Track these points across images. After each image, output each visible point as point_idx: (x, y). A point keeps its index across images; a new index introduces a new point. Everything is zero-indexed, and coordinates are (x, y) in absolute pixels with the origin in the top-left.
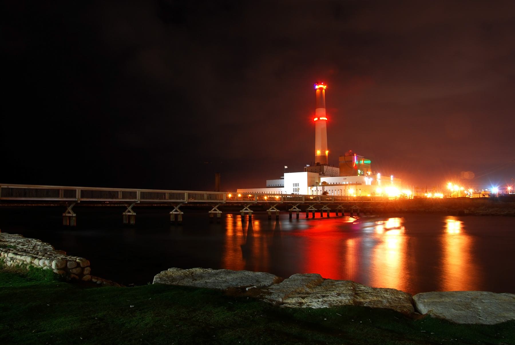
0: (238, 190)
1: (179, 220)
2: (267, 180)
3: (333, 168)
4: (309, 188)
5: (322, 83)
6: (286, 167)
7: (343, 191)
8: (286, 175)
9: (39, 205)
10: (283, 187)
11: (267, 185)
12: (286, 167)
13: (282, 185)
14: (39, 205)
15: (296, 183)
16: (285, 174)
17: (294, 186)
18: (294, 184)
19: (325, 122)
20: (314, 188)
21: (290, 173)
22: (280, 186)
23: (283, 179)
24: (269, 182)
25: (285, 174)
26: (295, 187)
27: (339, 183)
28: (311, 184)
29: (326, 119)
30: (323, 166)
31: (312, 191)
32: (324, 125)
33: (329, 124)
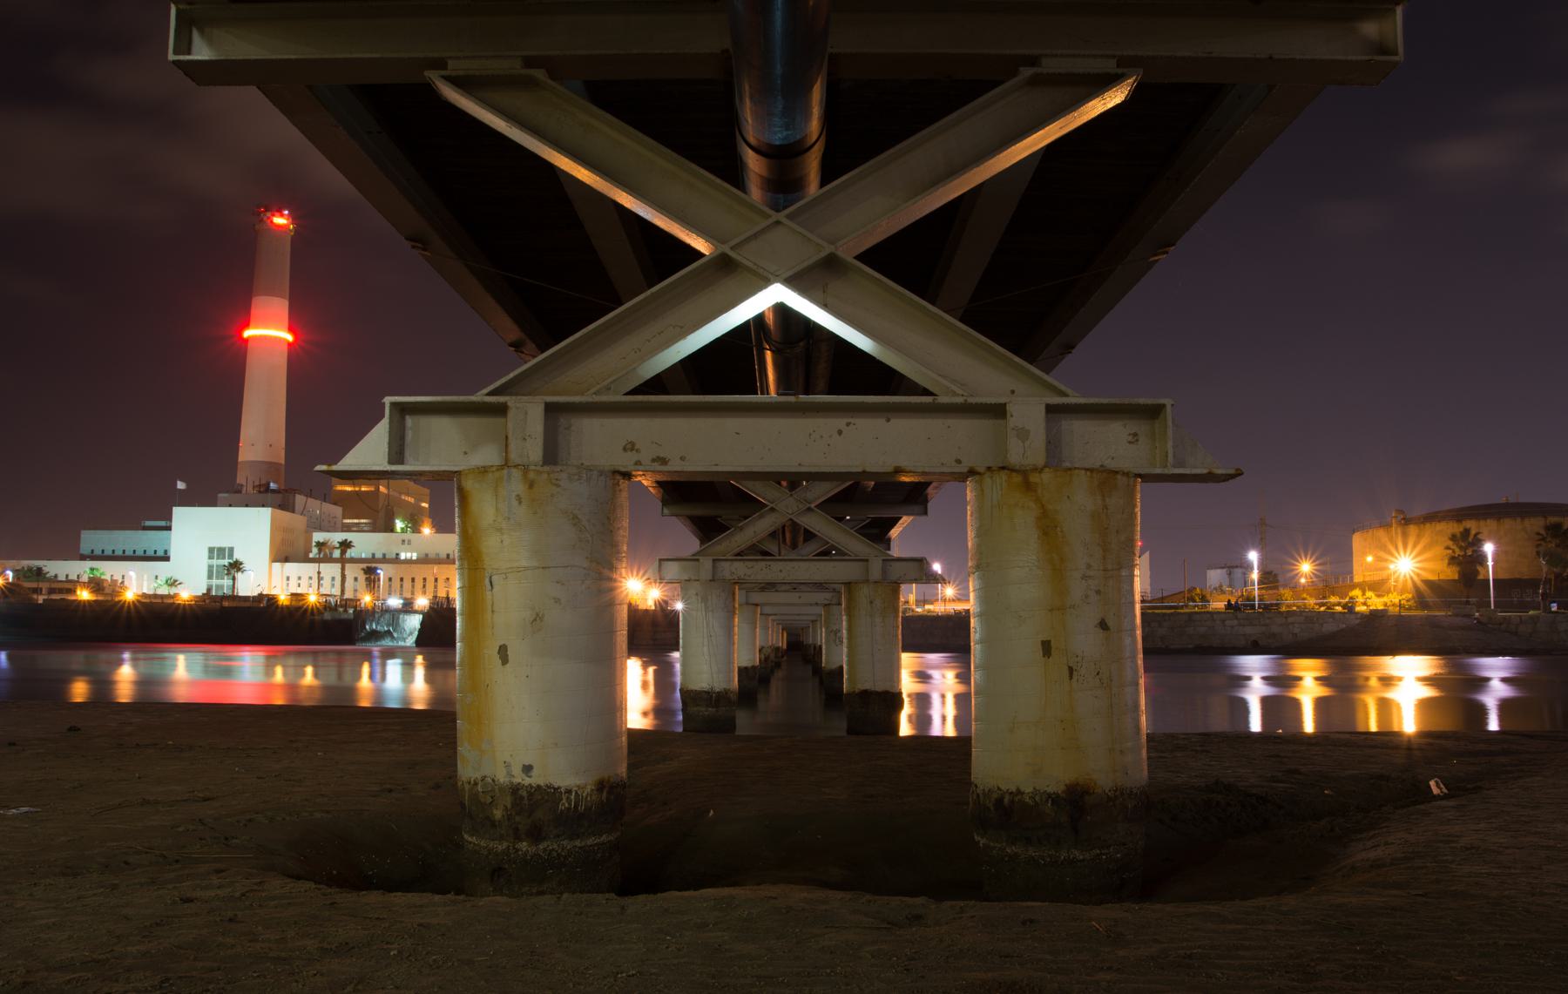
0: (1358, 541)
1: (936, 730)
2: (85, 529)
3: (324, 503)
4: (277, 565)
5: (286, 212)
6: (181, 485)
7: (441, 583)
8: (183, 516)
9: (457, 510)
10: (166, 558)
11: (85, 548)
12: (181, 485)
13: (160, 553)
14: (457, 510)
15: (223, 545)
16: (179, 513)
17: (211, 557)
18: (211, 550)
19: (285, 348)
20: (292, 568)
21: (199, 506)
22: (152, 554)
23: (169, 528)
24: (91, 539)
25: (179, 513)
26: (215, 562)
27: (384, 555)
28: (284, 553)
29: (290, 338)
30: (294, 496)
31: (288, 579)
32: (281, 360)
33: (297, 359)
